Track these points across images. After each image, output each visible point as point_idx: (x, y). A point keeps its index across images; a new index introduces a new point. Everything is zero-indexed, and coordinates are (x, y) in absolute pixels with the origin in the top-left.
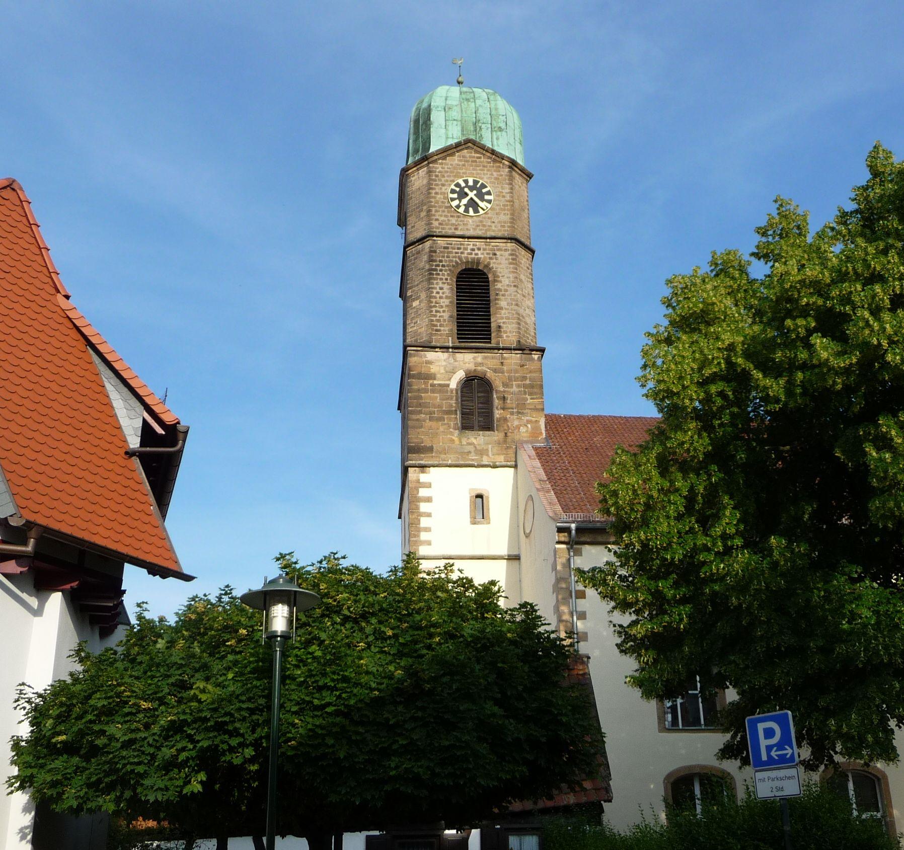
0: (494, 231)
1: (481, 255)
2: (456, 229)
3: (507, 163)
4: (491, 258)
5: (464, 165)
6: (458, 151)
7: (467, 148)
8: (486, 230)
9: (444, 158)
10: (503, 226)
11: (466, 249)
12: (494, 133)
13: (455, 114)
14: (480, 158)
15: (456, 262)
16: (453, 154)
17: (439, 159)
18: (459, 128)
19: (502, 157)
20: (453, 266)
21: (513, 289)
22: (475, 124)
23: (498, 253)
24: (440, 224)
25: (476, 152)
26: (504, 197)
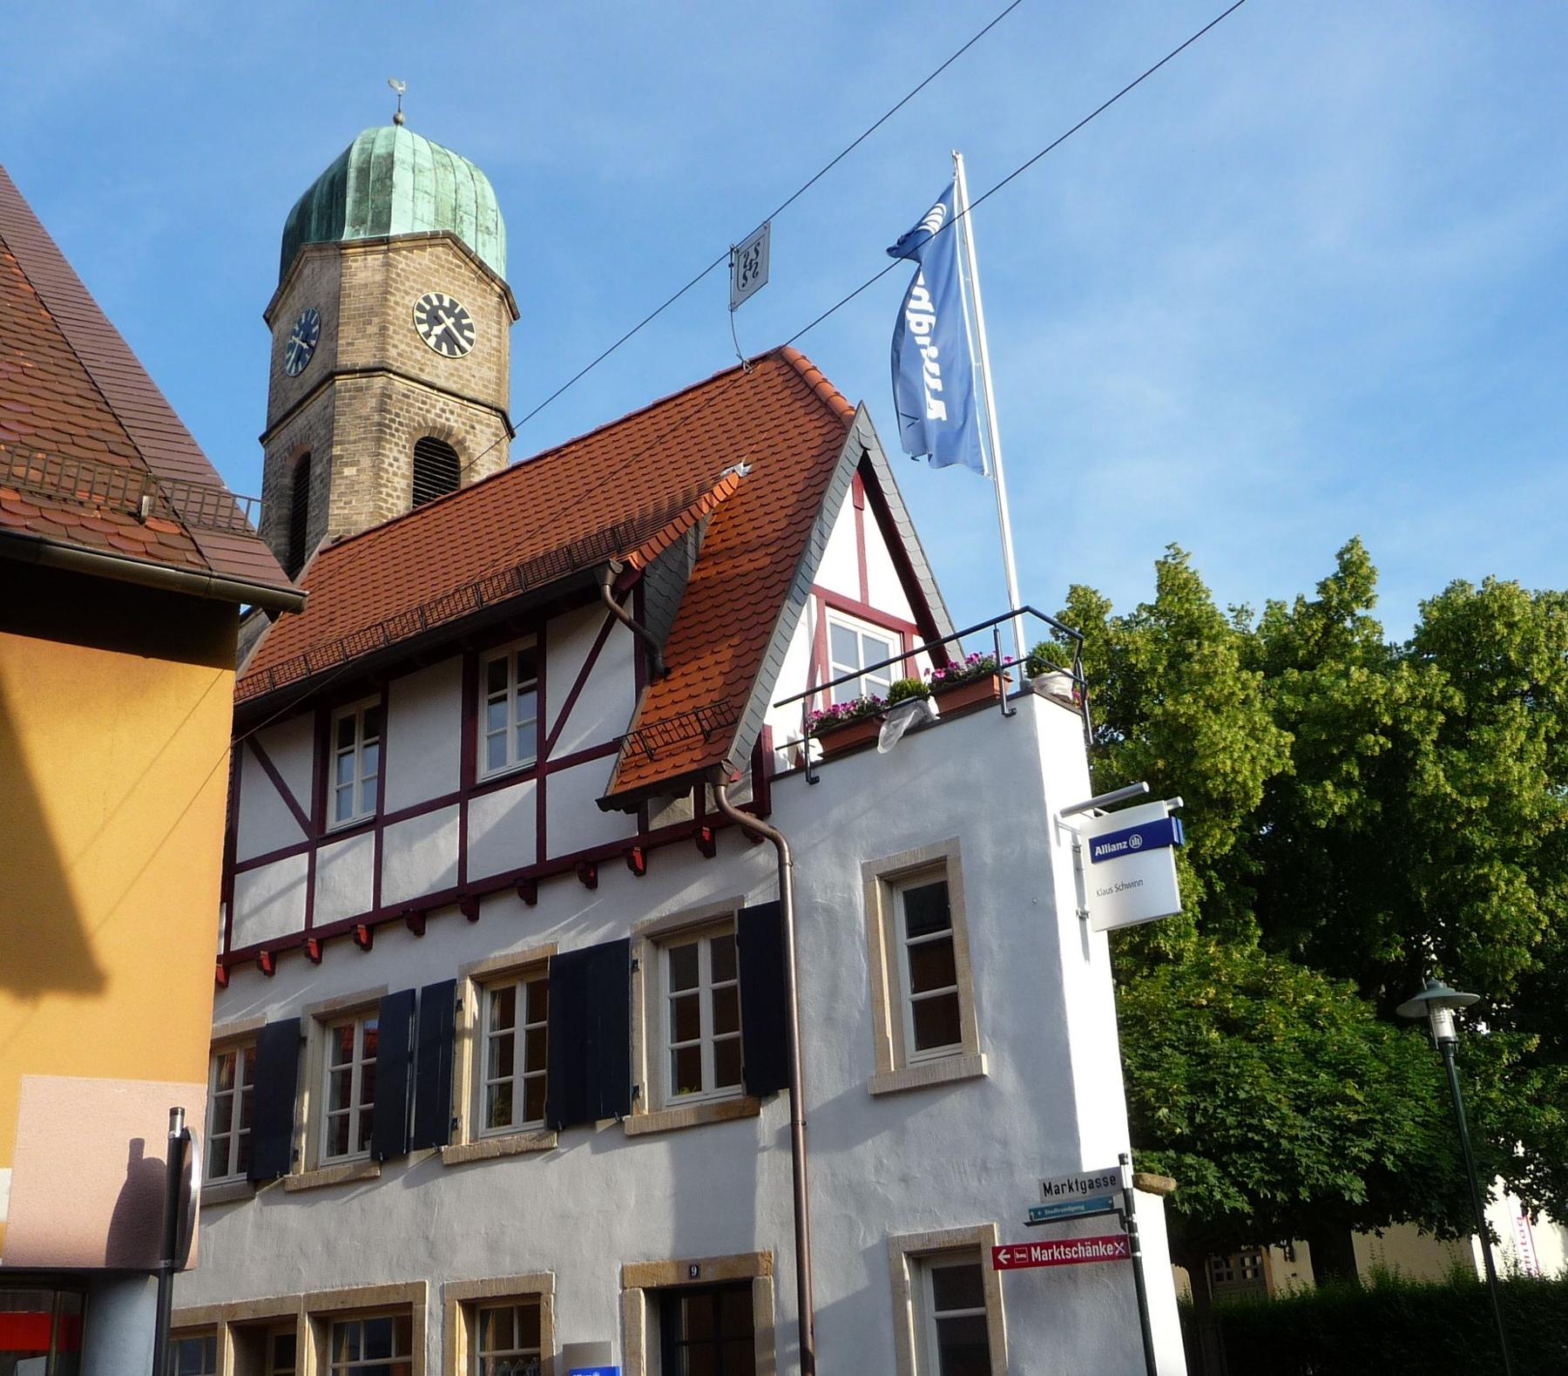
2: (421, 370)
7: (443, 245)
9: (410, 250)
11: (434, 407)
13: (427, 182)
16: (422, 248)
18: (433, 209)
19: (493, 278)
22: (455, 210)
25: (455, 255)
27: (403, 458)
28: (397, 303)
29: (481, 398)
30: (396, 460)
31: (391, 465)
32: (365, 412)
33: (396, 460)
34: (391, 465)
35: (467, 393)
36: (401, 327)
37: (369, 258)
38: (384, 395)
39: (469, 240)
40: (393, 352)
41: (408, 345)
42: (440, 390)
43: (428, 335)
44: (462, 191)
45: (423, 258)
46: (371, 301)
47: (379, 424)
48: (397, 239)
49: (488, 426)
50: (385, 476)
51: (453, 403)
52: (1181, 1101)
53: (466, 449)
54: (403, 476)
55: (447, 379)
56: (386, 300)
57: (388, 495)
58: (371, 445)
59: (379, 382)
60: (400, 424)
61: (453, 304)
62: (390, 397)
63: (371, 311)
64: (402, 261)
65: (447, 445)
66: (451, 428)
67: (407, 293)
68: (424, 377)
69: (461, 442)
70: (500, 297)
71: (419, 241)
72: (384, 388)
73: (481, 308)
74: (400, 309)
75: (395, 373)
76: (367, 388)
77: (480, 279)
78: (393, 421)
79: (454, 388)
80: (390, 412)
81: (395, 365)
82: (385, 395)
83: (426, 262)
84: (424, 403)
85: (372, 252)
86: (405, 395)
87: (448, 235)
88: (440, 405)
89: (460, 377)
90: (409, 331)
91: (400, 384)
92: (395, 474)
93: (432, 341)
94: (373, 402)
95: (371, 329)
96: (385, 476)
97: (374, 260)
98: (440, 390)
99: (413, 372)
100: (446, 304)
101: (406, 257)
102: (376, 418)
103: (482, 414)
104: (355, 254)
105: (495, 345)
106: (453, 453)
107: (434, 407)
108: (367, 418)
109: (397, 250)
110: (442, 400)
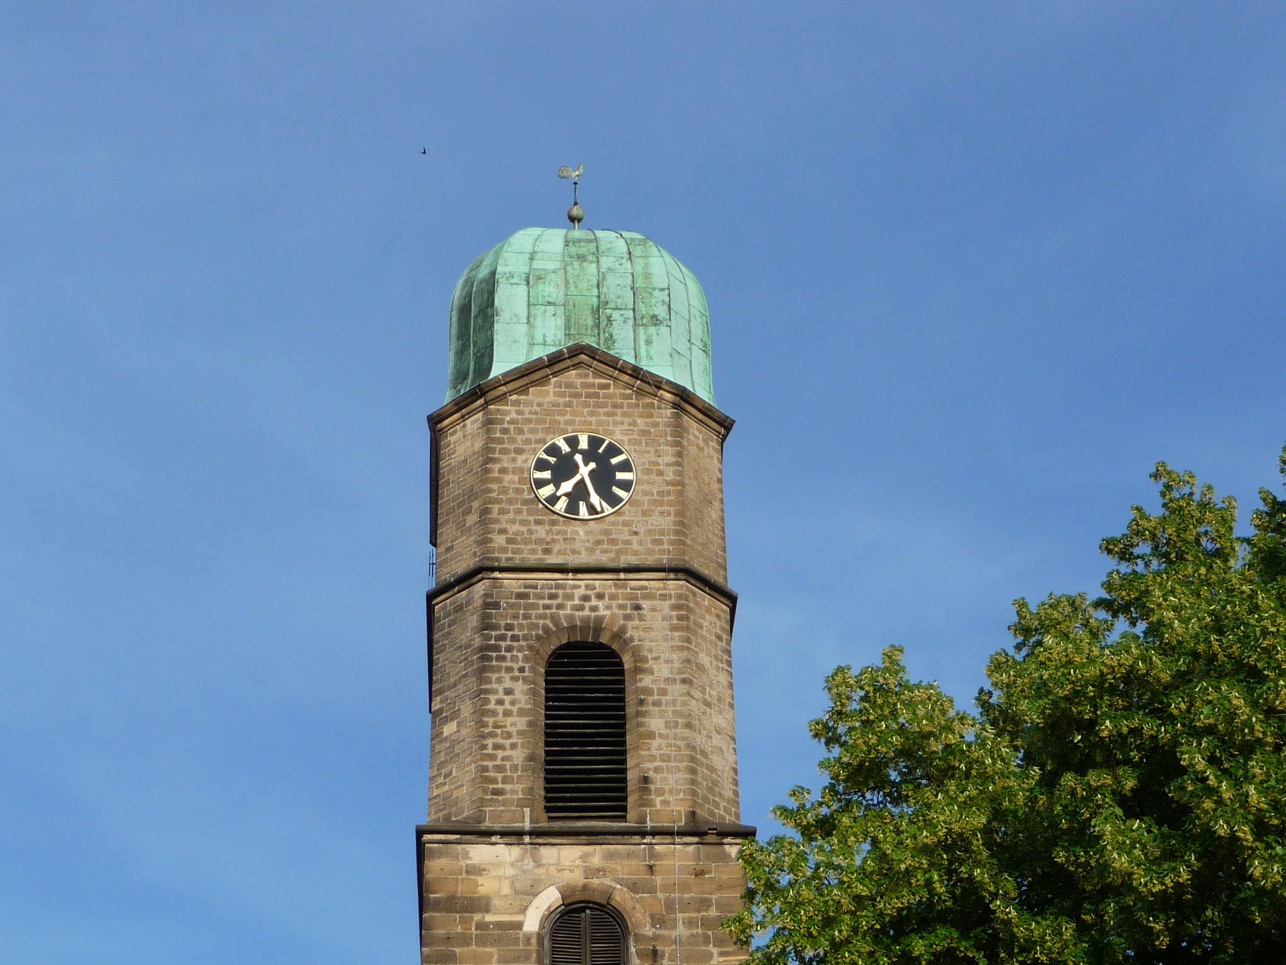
0: (636, 553)
1: (604, 610)
2: (547, 551)
3: (668, 396)
4: (628, 617)
5: (569, 405)
6: (555, 374)
7: (575, 366)
8: (619, 552)
9: (523, 390)
10: (659, 542)
11: (569, 597)
12: (641, 330)
13: (551, 290)
14: (607, 386)
15: (546, 630)
16: (543, 381)
17: (511, 392)
18: (560, 322)
19: (657, 383)
20: (539, 638)
21: (680, 688)
22: (596, 311)
23: (645, 604)
24: (509, 541)
25: (598, 374)
26: (660, 473)
27: (520, 687)
28: (503, 471)
29: (650, 561)
30: (508, 692)
31: (500, 702)
32: (464, 638)
33: (508, 692)
34: (500, 702)
35: (624, 561)
36: (510, 502)
37: (468, 422)
38: (486, 605)
39: (624, 352)
40: (499, 540)
41: (524, 523)
42: (577, 570)
43: (553, 499)
44: (611, 280)
45: (548, 394)
46: (471, 480)
47: (481, 649)
48: (498, 383)
49: (664, 597)
50: (490, 720)
51: (600, 583)
52: (875, 878)
53: (626, 643)
54: (522, 713)
55: (591, 551)
56: (487, 471)
57: (496, 747)
58: (471, 682)
59: (480, 588)
60: (515, 638)
61: (595, 442)
62: (496, 605)
63: (471, 494)
64: (508, 411)
65: (602, 646)
66: (599, 620)
67: (519, 451)
68: (553, 560)
69: (619, 635)
70: (675, 405)
71: (531, 374)
72: (486, 595)
73: (643, 433)
74: (508, 477)
75: (502, 570)
76: (468, 603)
77: (640, 392)
78: (502, 638)
79: (603, 559)
80: (495, 627)
81: (503, 558)
82: (490, 604)
83: (552, 398)
84: (552, 597)
85: (470, 413)
86: (521, 596)
87: (577, 350)
88: (582, 591)
89: (613, 542)
90: (525, 502)
91: (511, 582)
92: (507, 713)
93: (561, 505)
94: (473, 620)
95: (472, 519)
96: (490, 720)
97: (474, 423)
98: (577, 570)
99: (532, 559)
100: (584, 444)
101: (517, 403)
102: (478, 642)
103: (651, 583)
104: (453, 424)
105: (670, 476)
106: (614, 654)
107: (569, 597)
108: (468, 646)
109: (502, 398)
110: (580, 585)
